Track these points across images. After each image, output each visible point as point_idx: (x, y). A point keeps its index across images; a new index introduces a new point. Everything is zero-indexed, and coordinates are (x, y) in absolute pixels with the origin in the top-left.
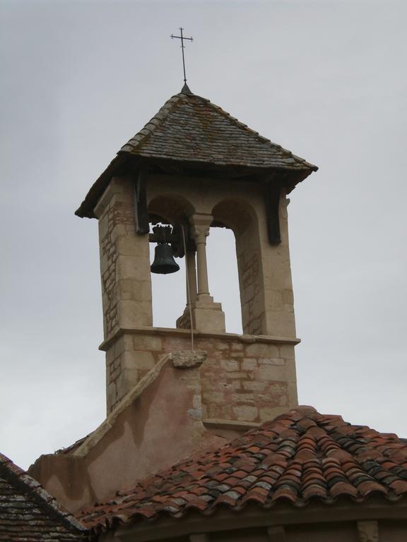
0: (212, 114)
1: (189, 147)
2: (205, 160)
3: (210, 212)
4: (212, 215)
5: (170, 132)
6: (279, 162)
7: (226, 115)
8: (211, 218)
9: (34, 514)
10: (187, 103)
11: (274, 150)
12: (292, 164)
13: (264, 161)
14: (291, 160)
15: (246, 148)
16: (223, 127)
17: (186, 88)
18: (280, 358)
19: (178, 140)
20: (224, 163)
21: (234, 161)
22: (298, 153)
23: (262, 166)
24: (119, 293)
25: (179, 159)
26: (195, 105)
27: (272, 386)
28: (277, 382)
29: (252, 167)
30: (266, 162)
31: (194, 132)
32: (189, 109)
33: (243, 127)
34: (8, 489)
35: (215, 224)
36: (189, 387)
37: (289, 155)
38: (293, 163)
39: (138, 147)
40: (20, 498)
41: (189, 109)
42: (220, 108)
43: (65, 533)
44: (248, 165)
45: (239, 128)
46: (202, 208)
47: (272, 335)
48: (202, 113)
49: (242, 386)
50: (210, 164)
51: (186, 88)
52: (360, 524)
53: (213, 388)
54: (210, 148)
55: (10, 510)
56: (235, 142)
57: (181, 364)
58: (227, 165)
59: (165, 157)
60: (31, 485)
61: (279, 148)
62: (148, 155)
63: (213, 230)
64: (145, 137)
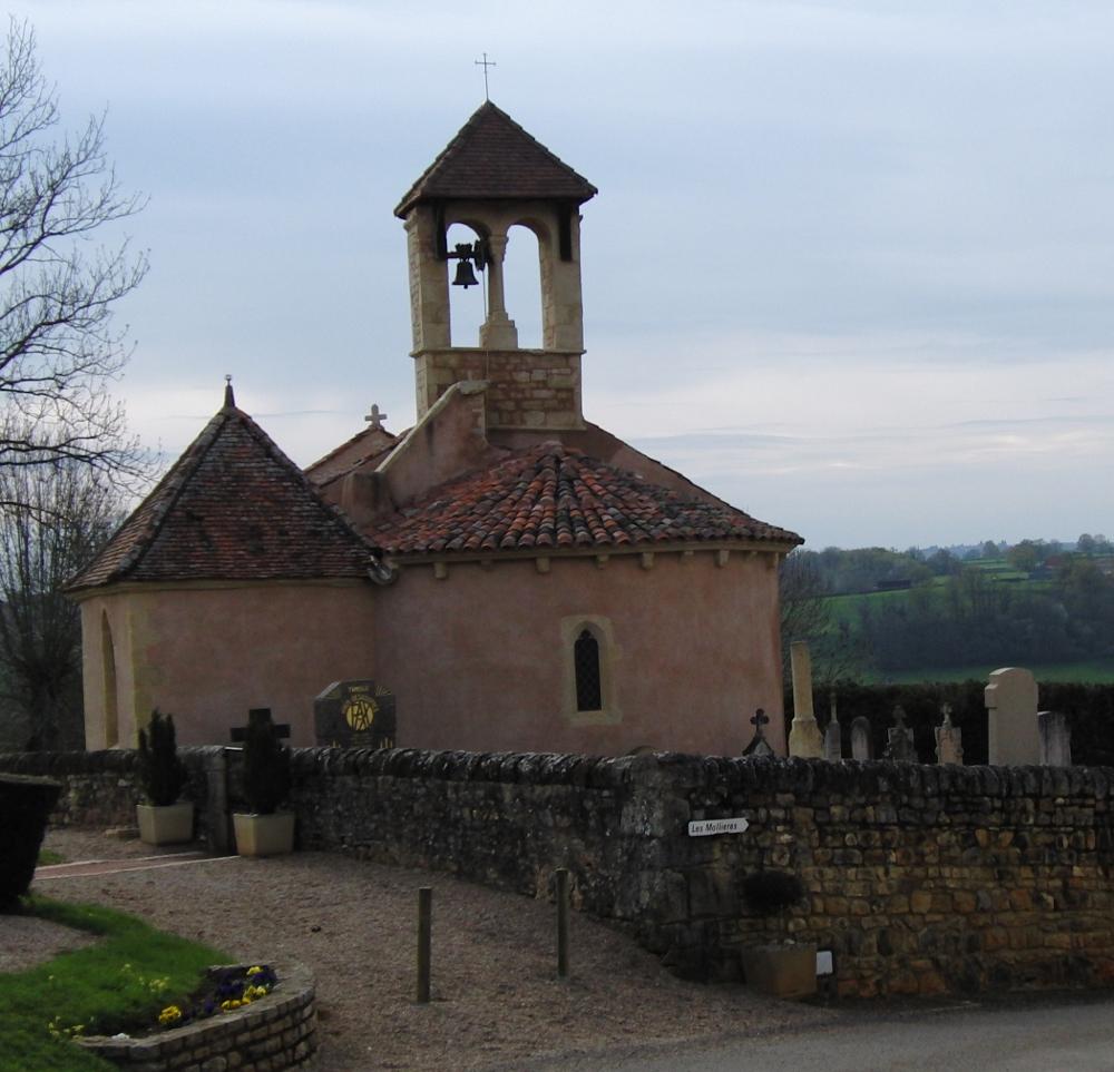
24: (433, 313)
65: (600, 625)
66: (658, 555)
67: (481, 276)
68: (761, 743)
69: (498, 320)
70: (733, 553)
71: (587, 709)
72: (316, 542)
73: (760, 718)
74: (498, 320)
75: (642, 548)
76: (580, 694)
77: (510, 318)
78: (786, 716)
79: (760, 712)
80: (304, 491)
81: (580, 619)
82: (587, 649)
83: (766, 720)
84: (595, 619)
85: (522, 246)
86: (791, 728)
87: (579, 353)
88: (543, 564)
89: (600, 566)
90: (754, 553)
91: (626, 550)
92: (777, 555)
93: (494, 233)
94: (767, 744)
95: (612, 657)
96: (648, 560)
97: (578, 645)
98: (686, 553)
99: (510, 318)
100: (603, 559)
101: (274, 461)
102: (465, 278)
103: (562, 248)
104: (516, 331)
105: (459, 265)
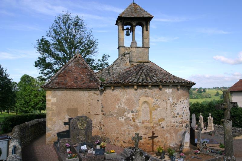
6: (147, 16)
14: (149, 15)
37: (149, 14)
50: (134, 17)
51: (133, 2)
61: (174, 76)
67: (131, 34)
88: (135, 87)
102: (128, 34)
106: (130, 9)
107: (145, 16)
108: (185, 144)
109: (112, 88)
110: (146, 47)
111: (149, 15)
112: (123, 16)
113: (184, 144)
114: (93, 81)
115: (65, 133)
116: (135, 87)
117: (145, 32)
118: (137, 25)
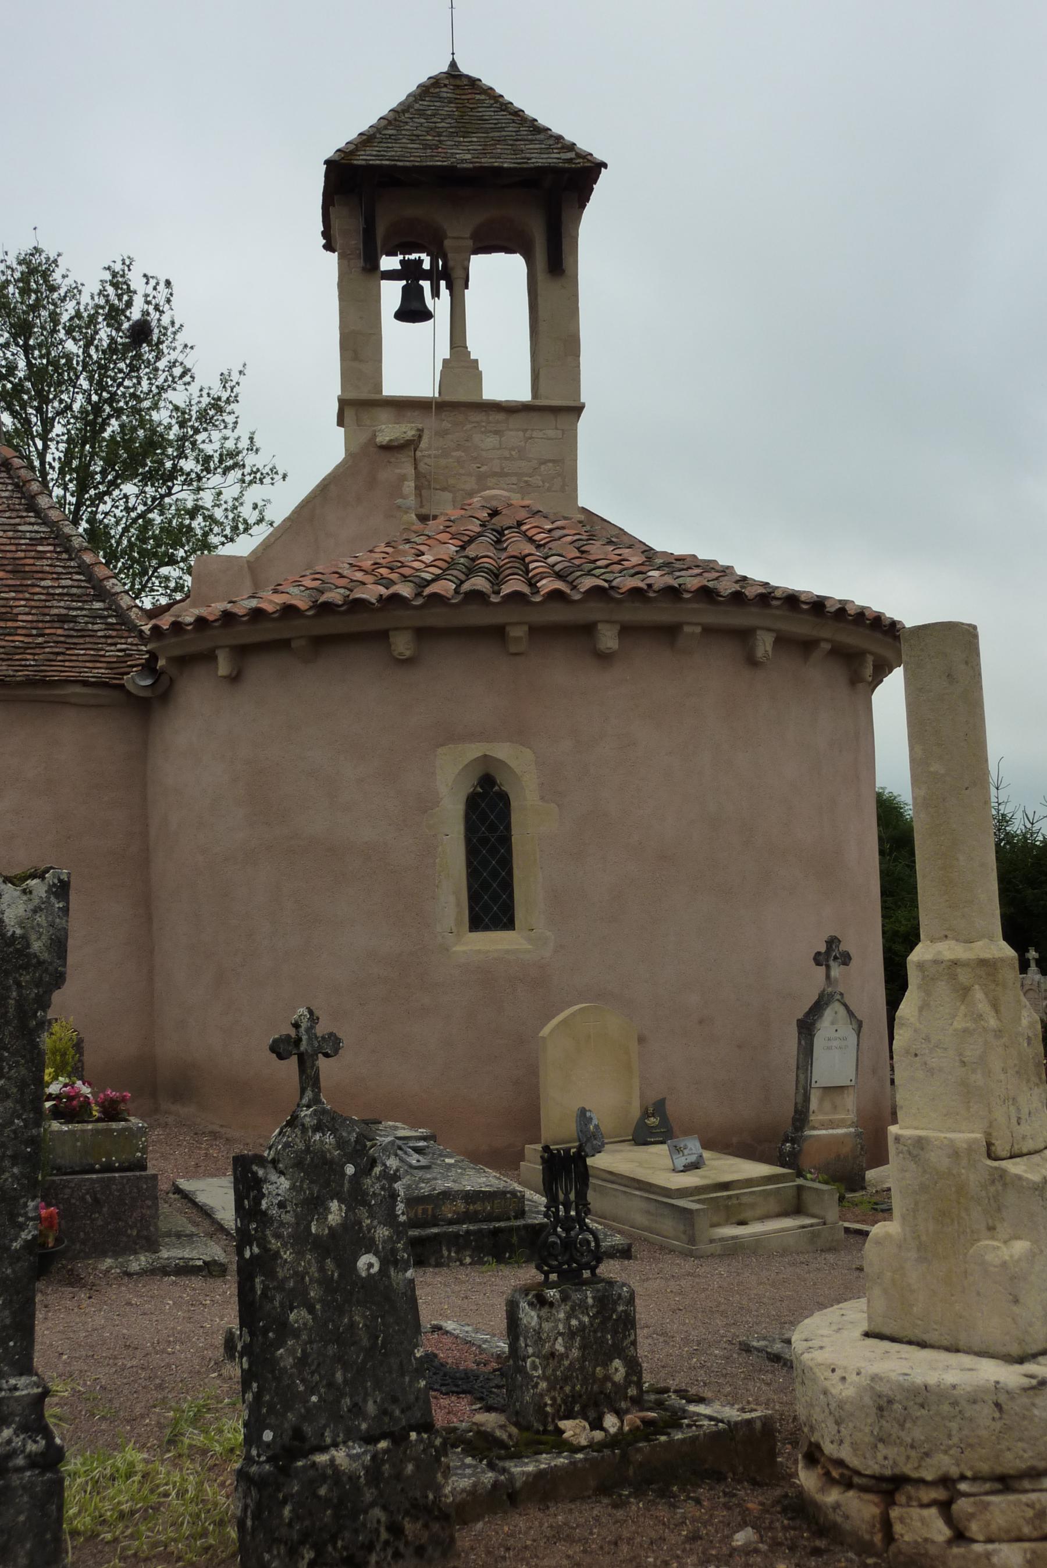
0: (478, 97)
1: (426, 147)
2: (445, 163)
3: (468, 235)
4: (471, 238)
5: (407, 127)
6: (554, 158)
7: (497, 98)
8: (470, 243)
9: (107, 624)
10: (445, 86)
11: (551, 142)
12: (570, 161)
13: (529, 159)
14: (572, 155)
15: (511, 142)
16: (488, 114)
17: (453, 64)
18: (557, 429)
19: (414, 138)
20: (471, 166)
21: (486, 161)
22: (584, 144)
23: (525, 166)
24: (359, 346)
25: (408, 164)
26: (457, 87)
27: (543, 467)
28: (550, 461)
29: (510, 168)
30: (533, 160)
31: (443, 124)
32: (454, 95)
33: (518, 113)
34: (88, 595)
35: (477, 251)
36: (398, 471)
37: (572, 147)
38: (571, 159)
39: (352, 153)
40: (97, 605)
41: (454, 95)
42: (491, 89)
43: (136, 645)
44: (505, 165)
45: (510, 114)
46: (457, 229)
47: (547, 398)
48: (463, 97)
49: (502, 468)
50: (452, 169)
51: (453, 64)
52: (391, 633)
53: (462, 471)
54: (458, 145)
55: (80, 620)
56: (498, 134)
57: (384, 443)
58: (475, 167)
59: (387, 163)
60: (113, 591)
61: (559, 138)
62: (363, 162)
63: (472, 257)
64: (367, 139)
65: (513, 764)
66: (627, 630)
67: (440, 305)
68: (836, 1006)
69: (460, 364)
70: (782, 641)
71: (487, 928)
72: (60, 632)
73: (831, 954)
74: (460, 364)
75: (595, 611)
76: (473, 897)
77: (472, 357)
78: (888, 1003)
79: (832, 942)
80: (70, 559)
81: (474, 751)
82: (488, 812)
83: (845, 959)
84: (502, 751)
85: (498, 281)
86: (904, 987)
87: (577, 410)
88: (402, 644)
89: (513, 649)
90: (826, 646)
91: (558, 614)
92: (870, 660)
93: (449, 234)
94: (845, 1006)
95: (533, 827)
96: (608, 639)
97: (473, 803)
98: (687, 629)
99: (472, 357)
100: (517, 632)
101: (38, 516)
102: (413, 311)
103: (554, 267)
104: (479, 375)
105: (404, 288)
106: (421, 113)
107: (539, 160)
108: (821, 1101)
109: (223, 667)
110: (555, 407)
111: (572, 155)
112: (360, 160)
113: (814, 1104)
114: (93, 634)
115: (803, 1042)
116: (402, 644)
117: (547, 287)
118: (489, 242)
